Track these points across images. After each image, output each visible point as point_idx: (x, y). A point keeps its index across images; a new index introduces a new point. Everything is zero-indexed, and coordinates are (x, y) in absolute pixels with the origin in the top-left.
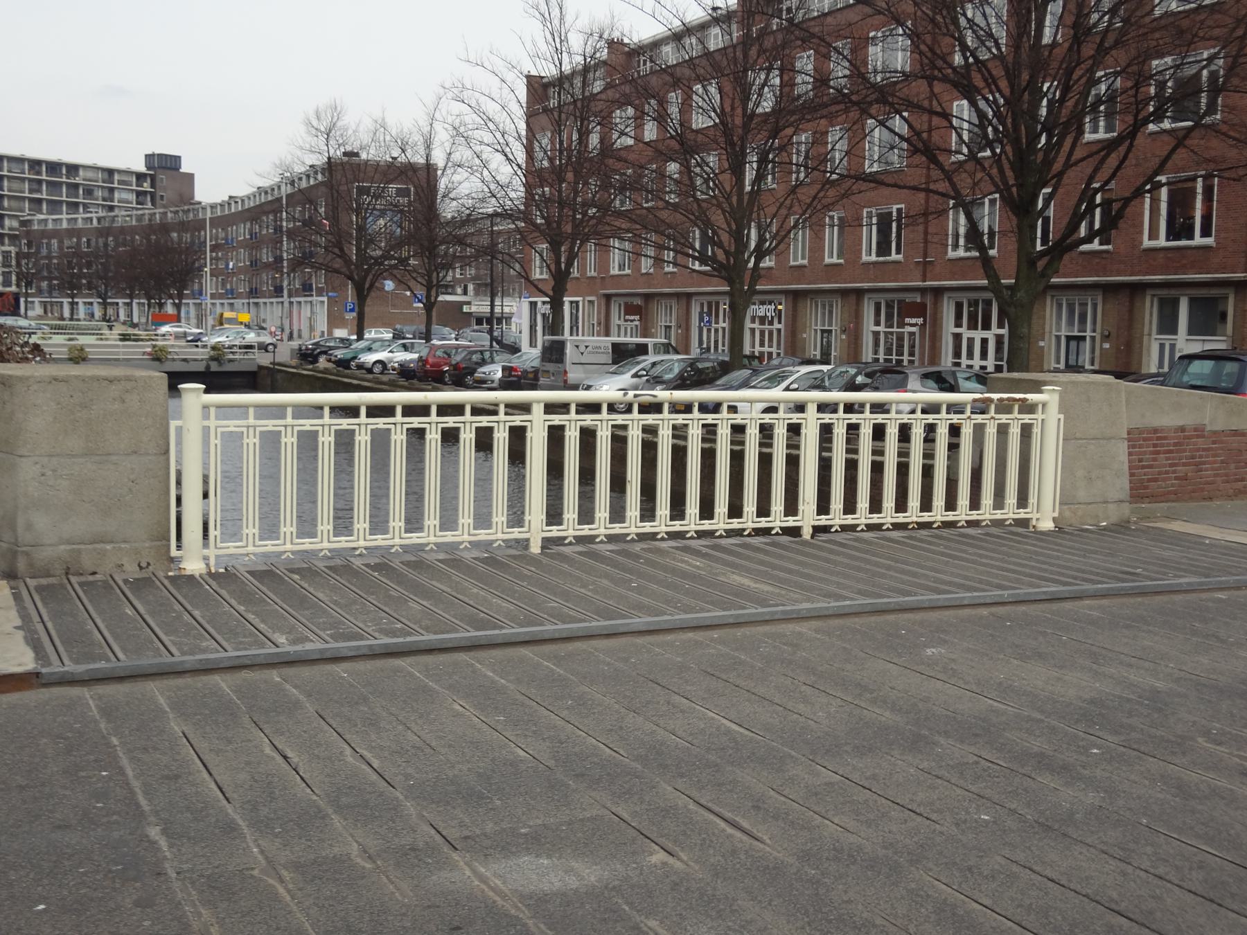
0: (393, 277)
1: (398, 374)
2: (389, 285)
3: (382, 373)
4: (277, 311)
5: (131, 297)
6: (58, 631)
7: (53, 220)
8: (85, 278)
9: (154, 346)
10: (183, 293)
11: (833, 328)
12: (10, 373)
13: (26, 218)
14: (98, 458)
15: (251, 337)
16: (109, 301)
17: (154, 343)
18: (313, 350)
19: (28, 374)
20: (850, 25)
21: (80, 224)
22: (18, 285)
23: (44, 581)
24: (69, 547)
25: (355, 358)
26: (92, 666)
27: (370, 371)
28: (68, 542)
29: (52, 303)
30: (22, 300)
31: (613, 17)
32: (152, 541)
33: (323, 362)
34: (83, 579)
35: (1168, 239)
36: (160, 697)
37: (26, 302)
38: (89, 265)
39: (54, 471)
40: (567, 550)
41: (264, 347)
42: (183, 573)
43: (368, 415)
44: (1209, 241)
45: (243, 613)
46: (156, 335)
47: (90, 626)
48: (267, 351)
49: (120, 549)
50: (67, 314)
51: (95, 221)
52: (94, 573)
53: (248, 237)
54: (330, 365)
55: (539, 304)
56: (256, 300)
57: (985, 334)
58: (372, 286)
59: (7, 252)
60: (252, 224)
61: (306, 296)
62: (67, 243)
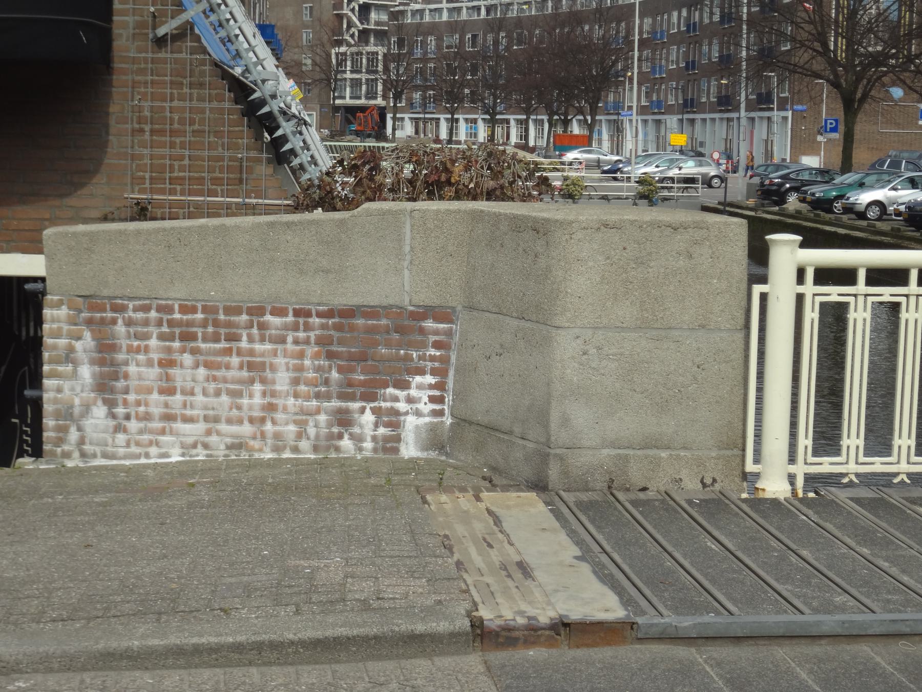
0: (902, 83)
1: (905, 220)
2: (897, 92)
3: (879, 219)
4: (721, 130)
5: (528, 111)
6: (631, 566)
7: (431, 10)
8: (469, 86)
9: (566, 179)
10: (597, 107)
12: (545, 215)
13: (397, 9)
14: (654, 333)
15: (690, 168)
16: (498, 117)
17: (565, 174)
18: (781, 185)
19: (571, 217)
21: (464, 15)
22: (385, 97)
23: (584, 497)
24: (614, 452)
25: (840, 197)
26: (699, 619)
27: (862, 215)
28: (613, 445)
29: (425, 121)
30: (389, 116)
32: (720, 448)
33: (793, 202)
34: (632, 496)
36: (802, 673)
37: (394, 119)
38: (474, 70)
39: (599, 348)
40: (842, 495)
41: (708, 182)
42: (761, 495)
43: (870, 282)
45: (870, 558)
46: (563, 163)
47: (669, 563)
48: (710, 186)
49: (678, 457)
50: (444, 135)
51: (483, 11)
52: (644, 489)
53: (683, 28)
54: (804, 207)
56: (691, 116)
58: (865, 96)
59: (373, 53)
60: (689, 12)
61: (721, 111)
62: (446, 41)
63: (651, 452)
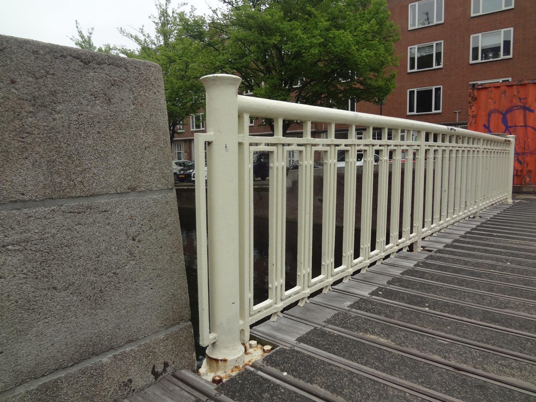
11: (182, 152)
20: (334, 18)
31: (137, 39)
32: (167, 327)
49: (124, 355)
63: (88, 364)
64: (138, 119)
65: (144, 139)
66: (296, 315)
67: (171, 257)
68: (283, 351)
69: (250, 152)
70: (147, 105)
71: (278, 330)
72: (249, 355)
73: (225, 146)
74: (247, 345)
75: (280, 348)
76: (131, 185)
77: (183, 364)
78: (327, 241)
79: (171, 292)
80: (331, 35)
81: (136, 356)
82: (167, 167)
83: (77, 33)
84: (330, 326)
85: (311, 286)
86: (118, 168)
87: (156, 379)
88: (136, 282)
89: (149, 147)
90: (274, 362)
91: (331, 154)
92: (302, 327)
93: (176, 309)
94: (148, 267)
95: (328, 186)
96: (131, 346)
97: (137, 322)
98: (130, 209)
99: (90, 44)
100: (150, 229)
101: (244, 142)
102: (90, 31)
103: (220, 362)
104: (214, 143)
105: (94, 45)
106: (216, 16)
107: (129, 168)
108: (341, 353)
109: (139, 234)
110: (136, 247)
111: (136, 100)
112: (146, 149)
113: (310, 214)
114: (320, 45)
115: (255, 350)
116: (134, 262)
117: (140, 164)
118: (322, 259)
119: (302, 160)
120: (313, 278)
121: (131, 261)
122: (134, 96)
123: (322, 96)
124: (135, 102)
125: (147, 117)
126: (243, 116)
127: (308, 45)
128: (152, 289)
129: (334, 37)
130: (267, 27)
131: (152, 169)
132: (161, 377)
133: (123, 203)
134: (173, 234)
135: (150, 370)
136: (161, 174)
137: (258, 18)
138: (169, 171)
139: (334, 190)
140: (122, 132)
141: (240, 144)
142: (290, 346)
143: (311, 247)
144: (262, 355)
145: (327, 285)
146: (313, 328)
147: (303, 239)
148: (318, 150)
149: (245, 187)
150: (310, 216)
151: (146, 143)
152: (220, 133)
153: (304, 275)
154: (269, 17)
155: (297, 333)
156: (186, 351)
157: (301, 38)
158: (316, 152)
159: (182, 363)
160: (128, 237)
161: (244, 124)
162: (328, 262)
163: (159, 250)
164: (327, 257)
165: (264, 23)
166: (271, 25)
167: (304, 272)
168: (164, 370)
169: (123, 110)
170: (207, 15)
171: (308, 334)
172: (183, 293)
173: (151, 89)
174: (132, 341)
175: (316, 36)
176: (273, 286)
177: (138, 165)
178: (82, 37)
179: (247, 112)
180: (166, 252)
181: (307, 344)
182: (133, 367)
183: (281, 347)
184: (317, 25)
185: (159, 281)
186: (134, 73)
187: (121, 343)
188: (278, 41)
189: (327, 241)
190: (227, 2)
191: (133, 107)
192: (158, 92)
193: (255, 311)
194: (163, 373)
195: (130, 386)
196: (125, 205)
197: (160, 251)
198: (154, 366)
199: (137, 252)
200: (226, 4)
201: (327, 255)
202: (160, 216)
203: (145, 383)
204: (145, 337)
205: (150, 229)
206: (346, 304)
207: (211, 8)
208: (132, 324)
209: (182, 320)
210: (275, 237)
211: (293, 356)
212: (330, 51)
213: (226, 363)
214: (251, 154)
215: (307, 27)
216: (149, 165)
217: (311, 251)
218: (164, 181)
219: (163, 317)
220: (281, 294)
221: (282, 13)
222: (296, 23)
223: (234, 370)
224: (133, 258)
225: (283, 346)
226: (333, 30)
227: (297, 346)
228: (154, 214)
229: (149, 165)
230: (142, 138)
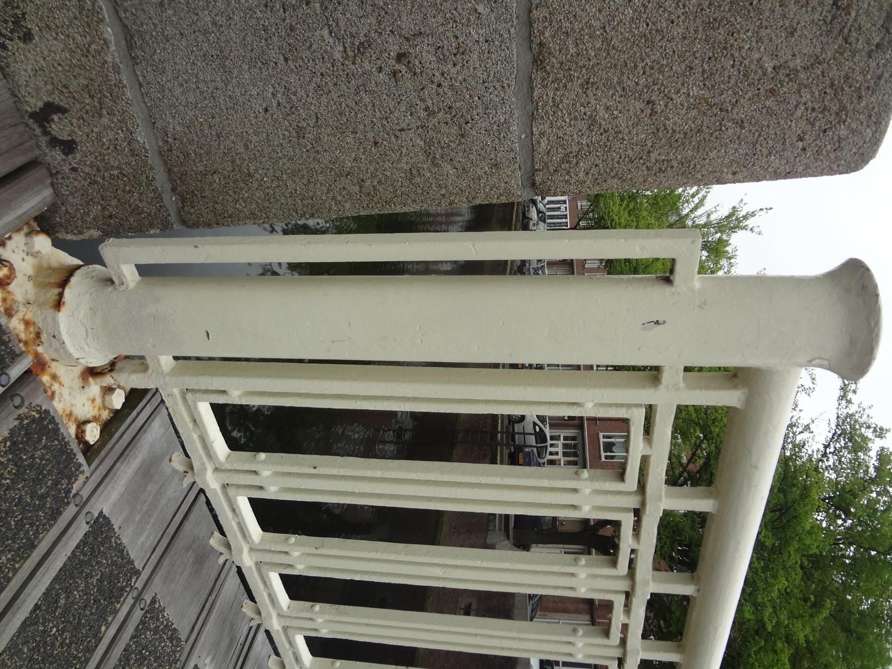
35: (603, 442)
44: (603, 459)
55: (565, 205)
57: (560, 454)
64: (733, 82)
65: (678, 100)
66: (187, 526)
67: (349, 174)
68: (68, 471)
69: (629, 406)
70: (770, 112)
71: (148, 471)
72: (78, 383)
73: (661, 320)
74: (108, 380)
75: (80, 465)
76: (550, 53)
77: (70, 199)
78: (372, 621)
79: (256, 170)
80: (779, 645)
81: (90, 58)
82: (594, 171)
83: (751, 210)
84: (138, 614)
85: (259, 570)
86: (600, 11)
87: (33, 115)
88: (286, 60)
89: (653, 112)
90: (29, 439)
91: (598, 646)
92: (148, 537)
93: (211, 184)
94: (324, 100)
95: (514, 634)
96: (117, 44)
97: (178, 60)
98: (485, 47)
99: (735, 228)
100: (426, 109)
101: (662, 387)
102: (756, 230)
103: (57, 291)
104: (668, 290)
105: (733, 235)
106: (800, 429)
107: (600, 49)
108: (26, 643)
109: (415, 74)
110: (379, 62)
111: (788, 75)
112: (648, 103)
113: (444, 579)
114: (761, 624)
115: (93, 400)
116: (338, 56)
117: (608, 84)
118: (328, 606)
119: (592, 566)
120: (282, 576)
121: (341, 49)
122: (797, 71)
123: (662, 622)
124: (782, 71)
125: (736, 110)
126: (736, 387)
127: (760, 600)
128: (266, 110)
129: (775, 652)
130: (788, 521)
131: (593, 121)
132: (38, 131)
133: (501, 27)
134: (410, 180)
135: (56, 99)
136: (575, 148)
137: (804, 506)
138: (581, 175)
139: (503, 649)
140: (700, 29)
141: (653, 373)
142: (85, 493)
143: (357, 578)
144: (70, 414)
145: (263, 615)
146: (138, 565)
147: (379, 556)
148: (615, 612)
149: (529, 389)
150: (438, 579)
151: (666, 106)
152: (700, 307)
153: (286, 553)
154: (808, 527)
155: (127, 520)
156: (104, 209)
157: (769, 585)
158: (608, 606)
159: (72, 194)
160: (408, 39)
161: (713, 389)
162: (320, 620)
163: (370, 135)
164: (332, 618)
165: (795, 517)
166: (792, 530)
167: (296, 554)
168: (54, 142)
169: (763, 33)
170: (801, 414)
171: (120, 550)
172: (254, 206)
173: (813, 125)
174: (130, 46)
175: (776, 615)
176: (261, 462)
177: (605, 76)
178: (745, 217)
179: (749, 401)
180: (363, 157)
181: (84, 542)
182: (62, 46)
183: (85, 467)
184: (797, 618)
185: (287, 133)
186: (863, 73)
187: (125, 11)
188: (765, 541)
189: (372, 621)
190: (826, 451)
191: (769, 66)
192: (804, 149)
193: (196, 407)
194: (49, 137)
195: (16, 34)
196: (495, 31)
197: (367, 139)
198: (63, 110)
199: (367, 66)
200: (822, 449)
201: (337, 618)
202: (460, 143)
203: (22, 82)
204: (140, 85)
205: (426, 109)
206: (208, 661)
207: (813, 421)
208: (173, 45)
209: (183, 200)
210: (388, 475)
211: (42, 497)
212: (749, 642)
213: (51, 308)
214: (624, 410)
215: (791, 598)
216: (602, 113)
217: (348, 577)
218: (557, 158)
219: (191, 142)
220: (239, 486)
221: (814, 550)
222: (797, 576)
223: (32, 329)
224: (350, 54)
225: (87, 474)
226: (789, 649)
227: (82, 516)
228: (467, 123)
229: (602, 113)
230: (679, 91)
